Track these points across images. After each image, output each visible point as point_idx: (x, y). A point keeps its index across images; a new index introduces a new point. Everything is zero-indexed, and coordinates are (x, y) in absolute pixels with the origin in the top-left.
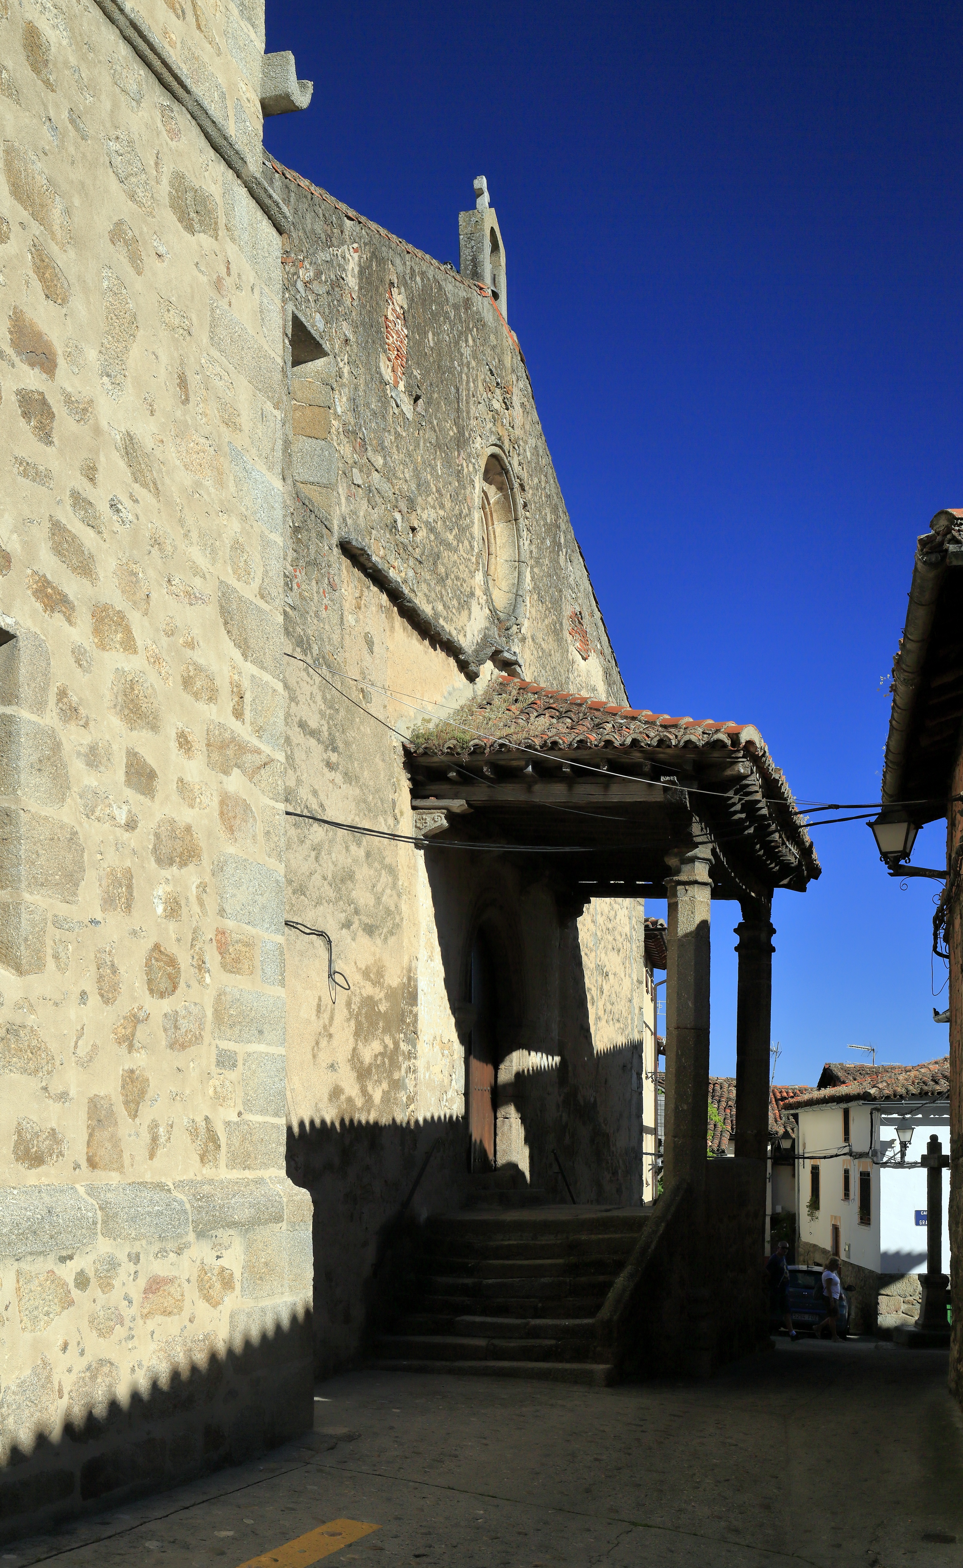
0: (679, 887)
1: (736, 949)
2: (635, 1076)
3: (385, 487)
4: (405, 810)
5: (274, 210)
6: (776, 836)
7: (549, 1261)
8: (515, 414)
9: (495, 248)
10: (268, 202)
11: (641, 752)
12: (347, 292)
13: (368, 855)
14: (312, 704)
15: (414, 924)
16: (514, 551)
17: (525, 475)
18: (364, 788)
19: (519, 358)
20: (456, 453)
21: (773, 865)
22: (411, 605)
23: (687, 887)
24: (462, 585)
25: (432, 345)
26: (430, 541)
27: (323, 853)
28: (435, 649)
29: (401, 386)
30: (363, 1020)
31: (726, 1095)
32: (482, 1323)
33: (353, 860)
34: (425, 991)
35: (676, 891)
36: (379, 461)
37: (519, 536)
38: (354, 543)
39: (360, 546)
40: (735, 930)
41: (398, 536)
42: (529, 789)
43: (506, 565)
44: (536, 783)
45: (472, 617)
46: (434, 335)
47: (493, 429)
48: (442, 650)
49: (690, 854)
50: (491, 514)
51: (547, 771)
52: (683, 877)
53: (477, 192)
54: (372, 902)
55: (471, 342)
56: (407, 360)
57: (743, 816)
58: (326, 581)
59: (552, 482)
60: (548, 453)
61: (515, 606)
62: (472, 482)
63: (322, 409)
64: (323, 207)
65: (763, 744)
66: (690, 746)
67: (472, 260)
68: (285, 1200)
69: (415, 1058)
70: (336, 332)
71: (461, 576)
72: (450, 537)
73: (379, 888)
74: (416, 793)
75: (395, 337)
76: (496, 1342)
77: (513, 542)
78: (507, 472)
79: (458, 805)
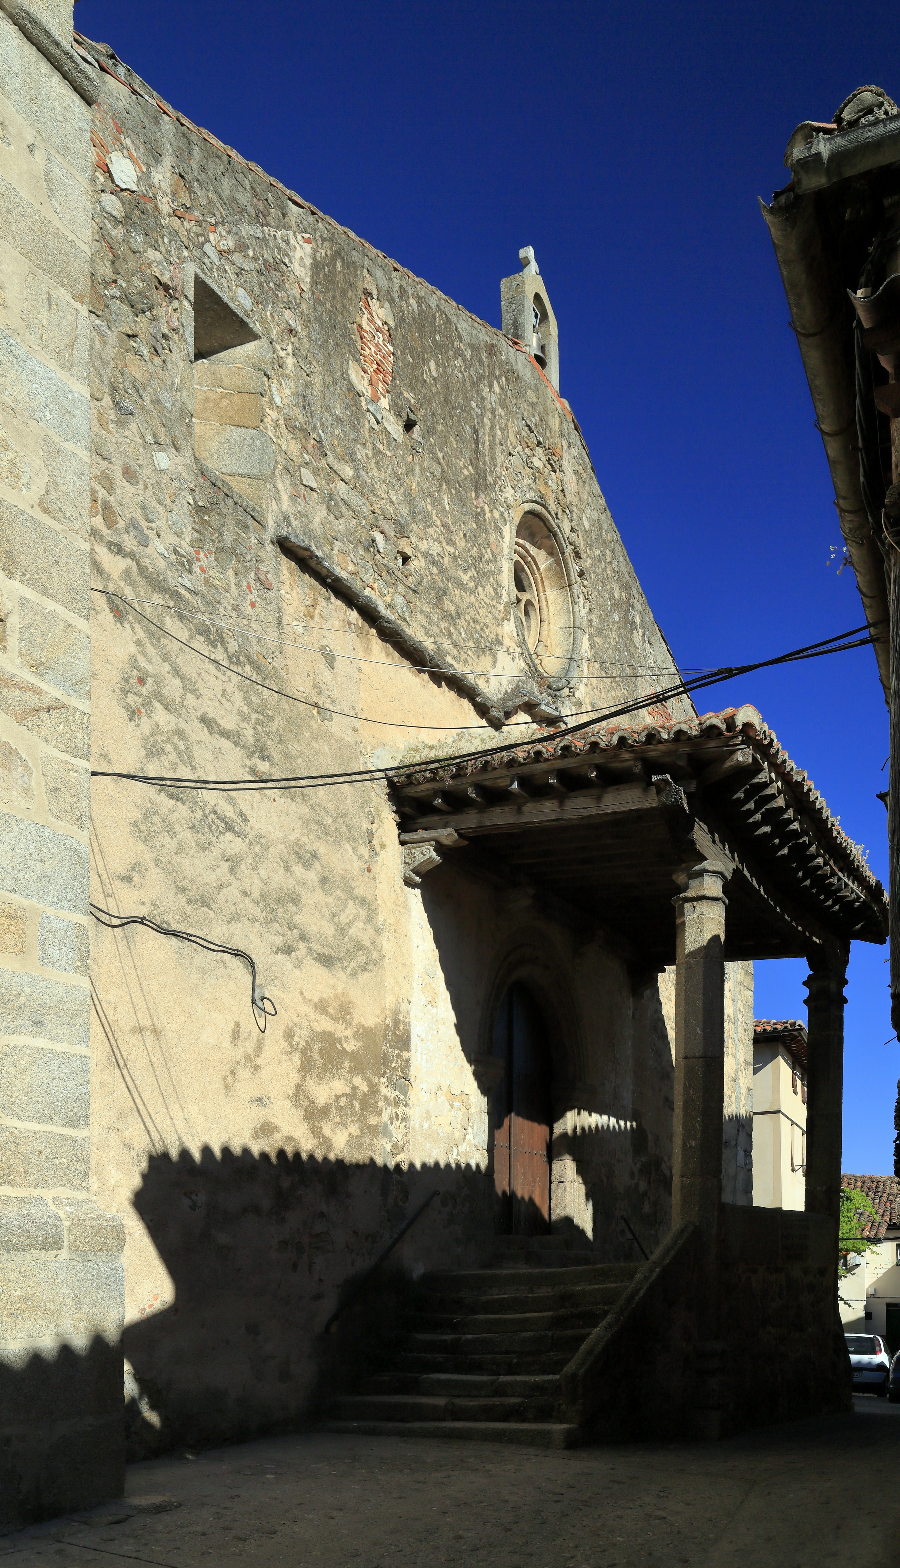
0: (686, 905)
1: (805, 1002)
2: (741, 1153)
3: (356, 500)
4: (388, 843)
5: (68, 66)
6: (820, 861)
7: (536, 1314)
8: (565, 479)
9: (543, 317)
10: (57, 52)
11: (631, 752)
12: (292, 280)
13: (324, 881)
14: (224, 701)
15: (404, 965)
16: (569, 618)
17: (581, 543)
18: (318, 809)
19: (573, 426)
20: (473, 495)
21: (830, 903)
22: (391, 626)
23: (695, 904)
24: (482, 629)
25: (435, 374)
26: (431, 574)
27: (243, 867)
28: (440, 686)
29: (384, 402)
30: (316, 1056)
31: (888, 1190)
32: (448, 1381)
33: (298, 883)
34: (423, 1036)
35: (683, 909)
36: (348, 472)
37: (574, 603)
38: (293, 539)
39: (302, 545)
40: (805, 983)
41: (378, 557)
42: (519, 811)
43: (561, 632)
44: (526, 803)
45: (498, 664)
46: (438, 365)
47: (533, 486)
48: (451, 688)
49: (697, 868)
50: (542, 580)
51: (535, 789)
52: (690, 894)
53: (524, 263)
54: (330, 931)
55: (497, 389)
56: (394, 379)
57: (767, 829)
58: (253, 575)
59: (621, 558)
60: (616, 529)
61: (568, 670)
62: (499, 531)
63: (253, 396)
64: (250, 178)
65: (766, 727)
66: (683, 738)
67: (513, 324)
68: (66, 1223)
69: (406, 1105)
70: (273, 317)
71: (482, 620)
72: (465, 578)
73: (343, 918)
74: (403, 827)
75: (373, 349)
76: (459, 1401)
77: (568, 608)
78: (555, 535)
79: (447, 835)
